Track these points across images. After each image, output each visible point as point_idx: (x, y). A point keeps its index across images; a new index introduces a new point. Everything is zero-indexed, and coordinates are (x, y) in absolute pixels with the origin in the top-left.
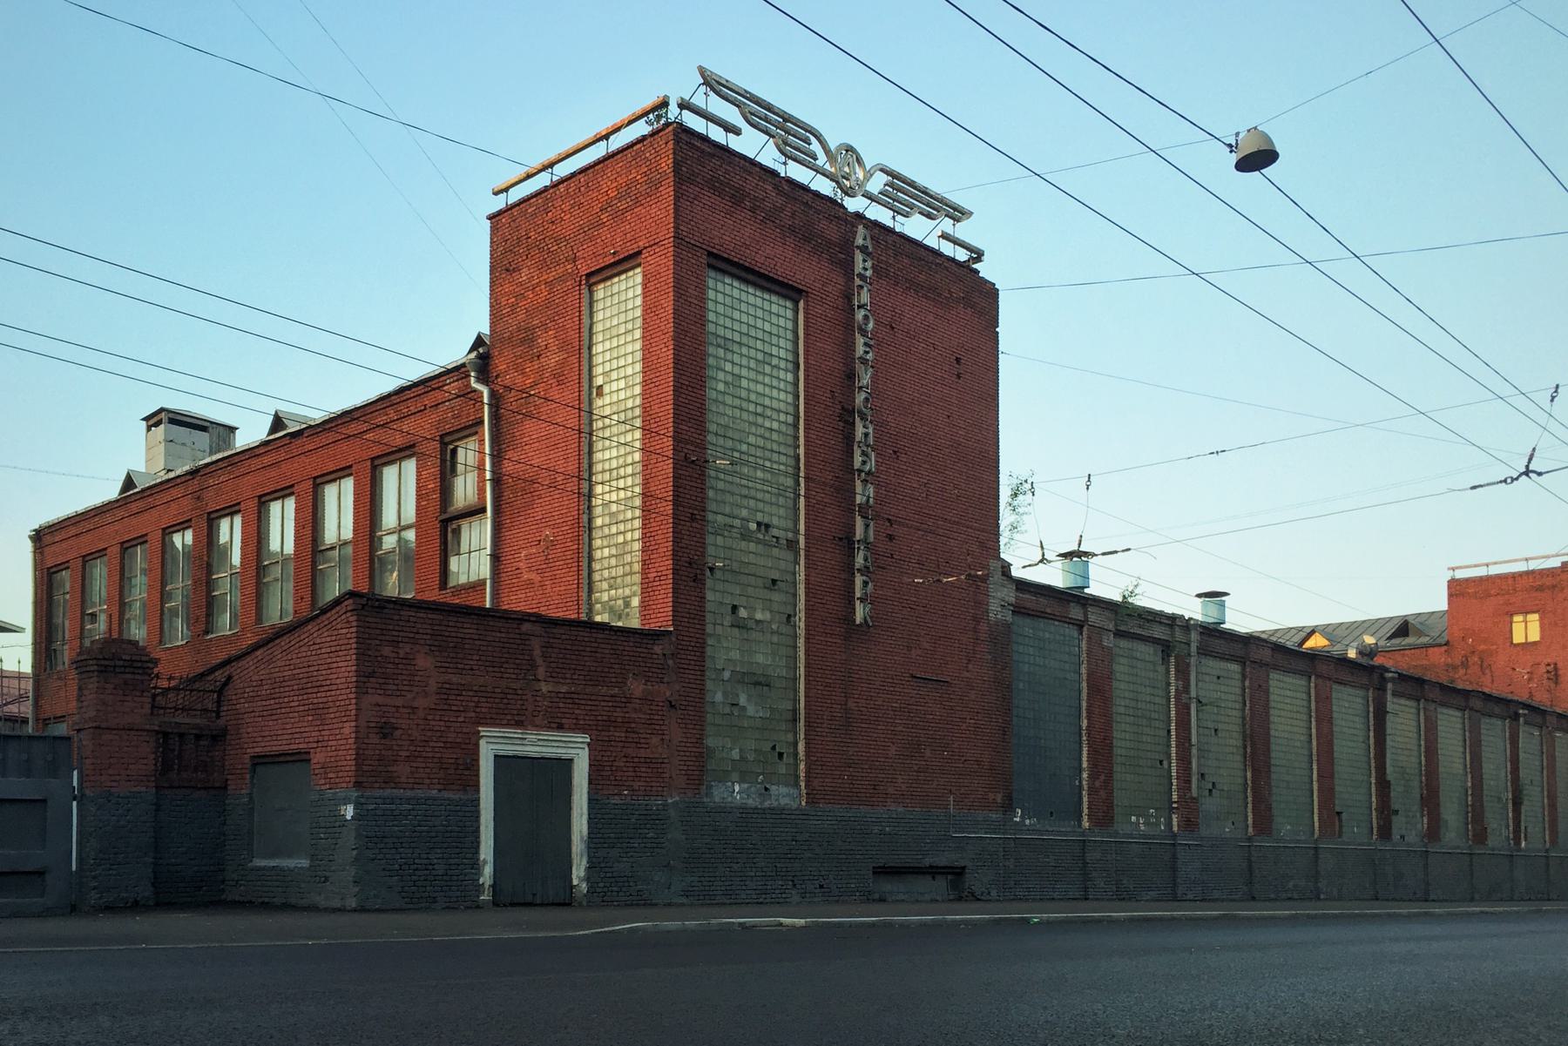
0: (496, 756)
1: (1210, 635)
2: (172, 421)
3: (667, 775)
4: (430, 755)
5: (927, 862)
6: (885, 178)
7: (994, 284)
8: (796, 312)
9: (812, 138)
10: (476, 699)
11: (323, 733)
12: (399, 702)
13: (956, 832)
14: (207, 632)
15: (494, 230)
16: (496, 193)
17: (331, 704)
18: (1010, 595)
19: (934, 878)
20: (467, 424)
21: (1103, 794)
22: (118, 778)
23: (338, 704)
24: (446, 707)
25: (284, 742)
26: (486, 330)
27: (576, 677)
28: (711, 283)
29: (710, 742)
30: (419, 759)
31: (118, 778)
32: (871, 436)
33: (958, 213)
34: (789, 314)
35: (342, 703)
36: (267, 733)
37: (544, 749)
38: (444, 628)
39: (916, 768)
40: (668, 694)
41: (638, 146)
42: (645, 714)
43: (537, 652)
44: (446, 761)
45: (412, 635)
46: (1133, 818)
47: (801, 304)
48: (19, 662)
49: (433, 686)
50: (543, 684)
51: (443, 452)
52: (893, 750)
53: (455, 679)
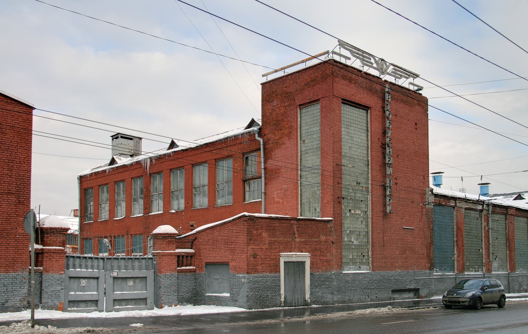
0: (284, 262)
1: (495, 207)
2: (122, 137)
3: (332, 265)
4: (266, 263)
5: (408, 287)
6: (392, 67)
7: (426, 98)
8: (367, 113)
9: (371, 58)
10: (279, 245)
11: (234, 257)
12: (258, 247)
13: (416, 277)
14: (192, 208)
15: (263, 89)
16: (263, 76)
17: (237, 248)
18: (432, 199)
19: (409, 292)
20: (253, 150)
21: (461, 262)
22: (167, 270)
23: (240, 248)
24: (271, 248)
25: (219, 259)
26: (258, 118)
27: (306, 236)
28: (342, 107)
29: (343, 254)
30: (264, 264)
31: (167, 270)
32: (391, 152)
33: (416, 76)
34: (365, 115)
35: (241, 248)
36: (212, 256)
37: (298, 259)
38: (270, 224)
39: (404, 258)
40: (332, 239)
41: (319, 66)
42: (325, 246)
43: (295, 229)
44: (271, 264)
45: (261, 227)
46: (471, 269)
47: (369, 111)
48: (105, 293)
49: (267, 242)
50: (297, 239)
51: (243, 158)
52: (397, 252)
53: (273, 239)
